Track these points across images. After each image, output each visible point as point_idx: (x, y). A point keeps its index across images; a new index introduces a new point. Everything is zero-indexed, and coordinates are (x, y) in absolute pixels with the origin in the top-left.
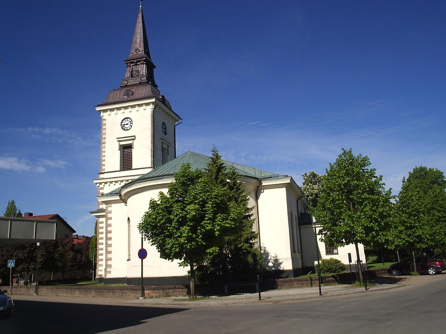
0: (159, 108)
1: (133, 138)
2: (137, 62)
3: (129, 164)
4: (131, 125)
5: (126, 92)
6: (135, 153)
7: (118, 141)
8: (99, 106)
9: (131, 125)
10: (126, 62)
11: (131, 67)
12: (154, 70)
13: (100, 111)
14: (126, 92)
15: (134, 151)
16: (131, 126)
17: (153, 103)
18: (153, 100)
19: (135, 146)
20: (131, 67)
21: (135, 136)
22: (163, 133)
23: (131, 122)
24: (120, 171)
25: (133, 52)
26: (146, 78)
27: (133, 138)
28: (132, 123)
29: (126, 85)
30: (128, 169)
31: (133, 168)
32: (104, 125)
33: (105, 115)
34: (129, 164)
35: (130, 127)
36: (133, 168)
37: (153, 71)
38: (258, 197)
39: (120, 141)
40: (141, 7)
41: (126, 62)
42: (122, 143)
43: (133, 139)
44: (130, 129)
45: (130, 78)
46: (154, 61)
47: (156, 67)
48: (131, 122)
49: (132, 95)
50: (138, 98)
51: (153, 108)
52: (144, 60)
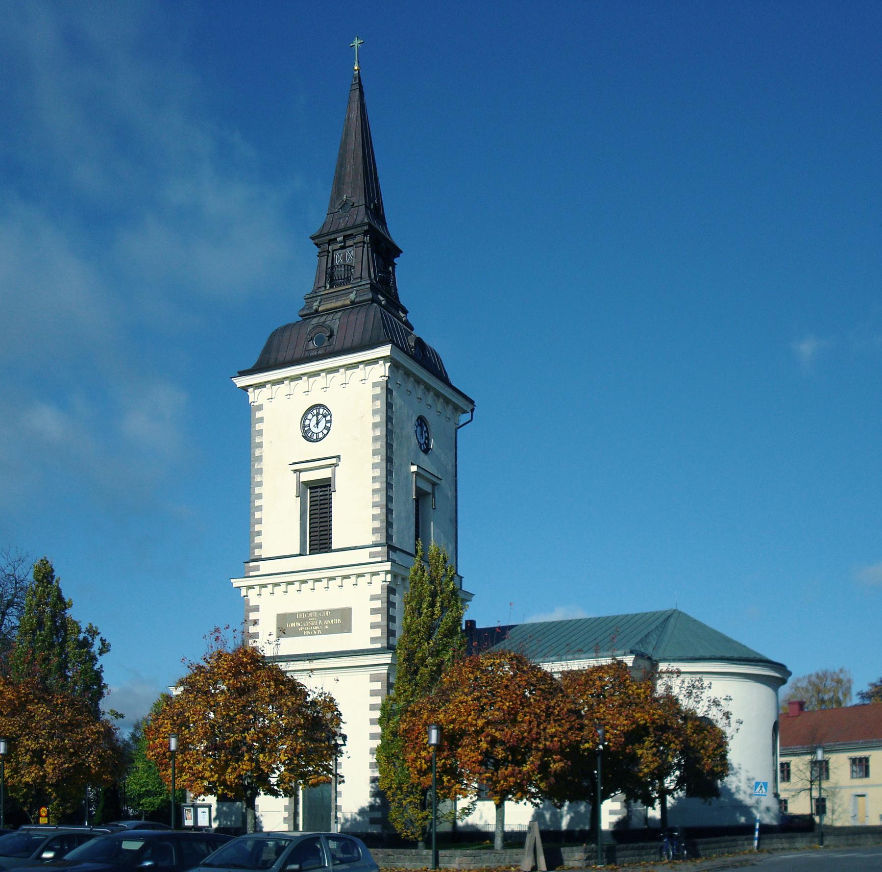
0: (405, 373)
1: (333, 461)
2: (346, 238)
3: (324, 541)
4: (328, 425)
5: (316, 331)
6: (338, 501)
7: (295, 471)
8: (243, 373)
9: (328, 425)
10: (316, 241)
11: (330, 255)
12: (396, 260)
13: (245, 389)
14: (316, 331)
15: (336, 499)
16: (328, 429)
17: (384, 358)
18: (385, 350)
19: (340, 484)
20: (330, 255)
21: (338, 457)
22: (421, 447)
23: (328, 418)
24: (300, 555)
25: (336, 210)
26: (369, 286)
27: (333, 461)
28: (330, 421)
29: (317, 311)
30: (322, 550)
31: (333, 548)
32: (377, 464)
33: (253, 396)
34: (324, 541)
35: (325, 432)
36: (333, 548)
37: (395, 264)
38: (752, 656)
39: (300, 471)
40: (356, 68)
41: (316, 241)
42: (306, 477)
43: (335, 465)
44: (325, 436)
45: (326, 289)
46: (396, 233)
47: (402, 252)
48: (328, 418)
49: (331, 336)
50: (345, 347)
51: (387, 375)
52: (365, 233)
